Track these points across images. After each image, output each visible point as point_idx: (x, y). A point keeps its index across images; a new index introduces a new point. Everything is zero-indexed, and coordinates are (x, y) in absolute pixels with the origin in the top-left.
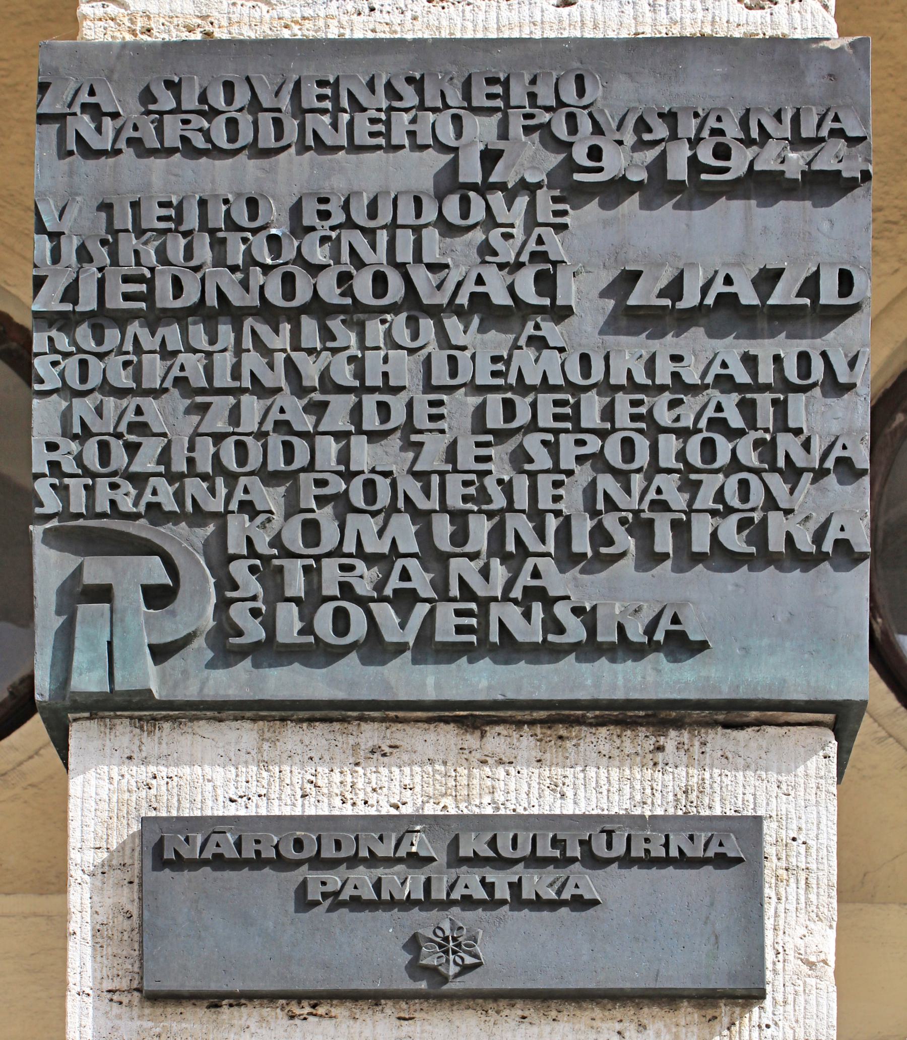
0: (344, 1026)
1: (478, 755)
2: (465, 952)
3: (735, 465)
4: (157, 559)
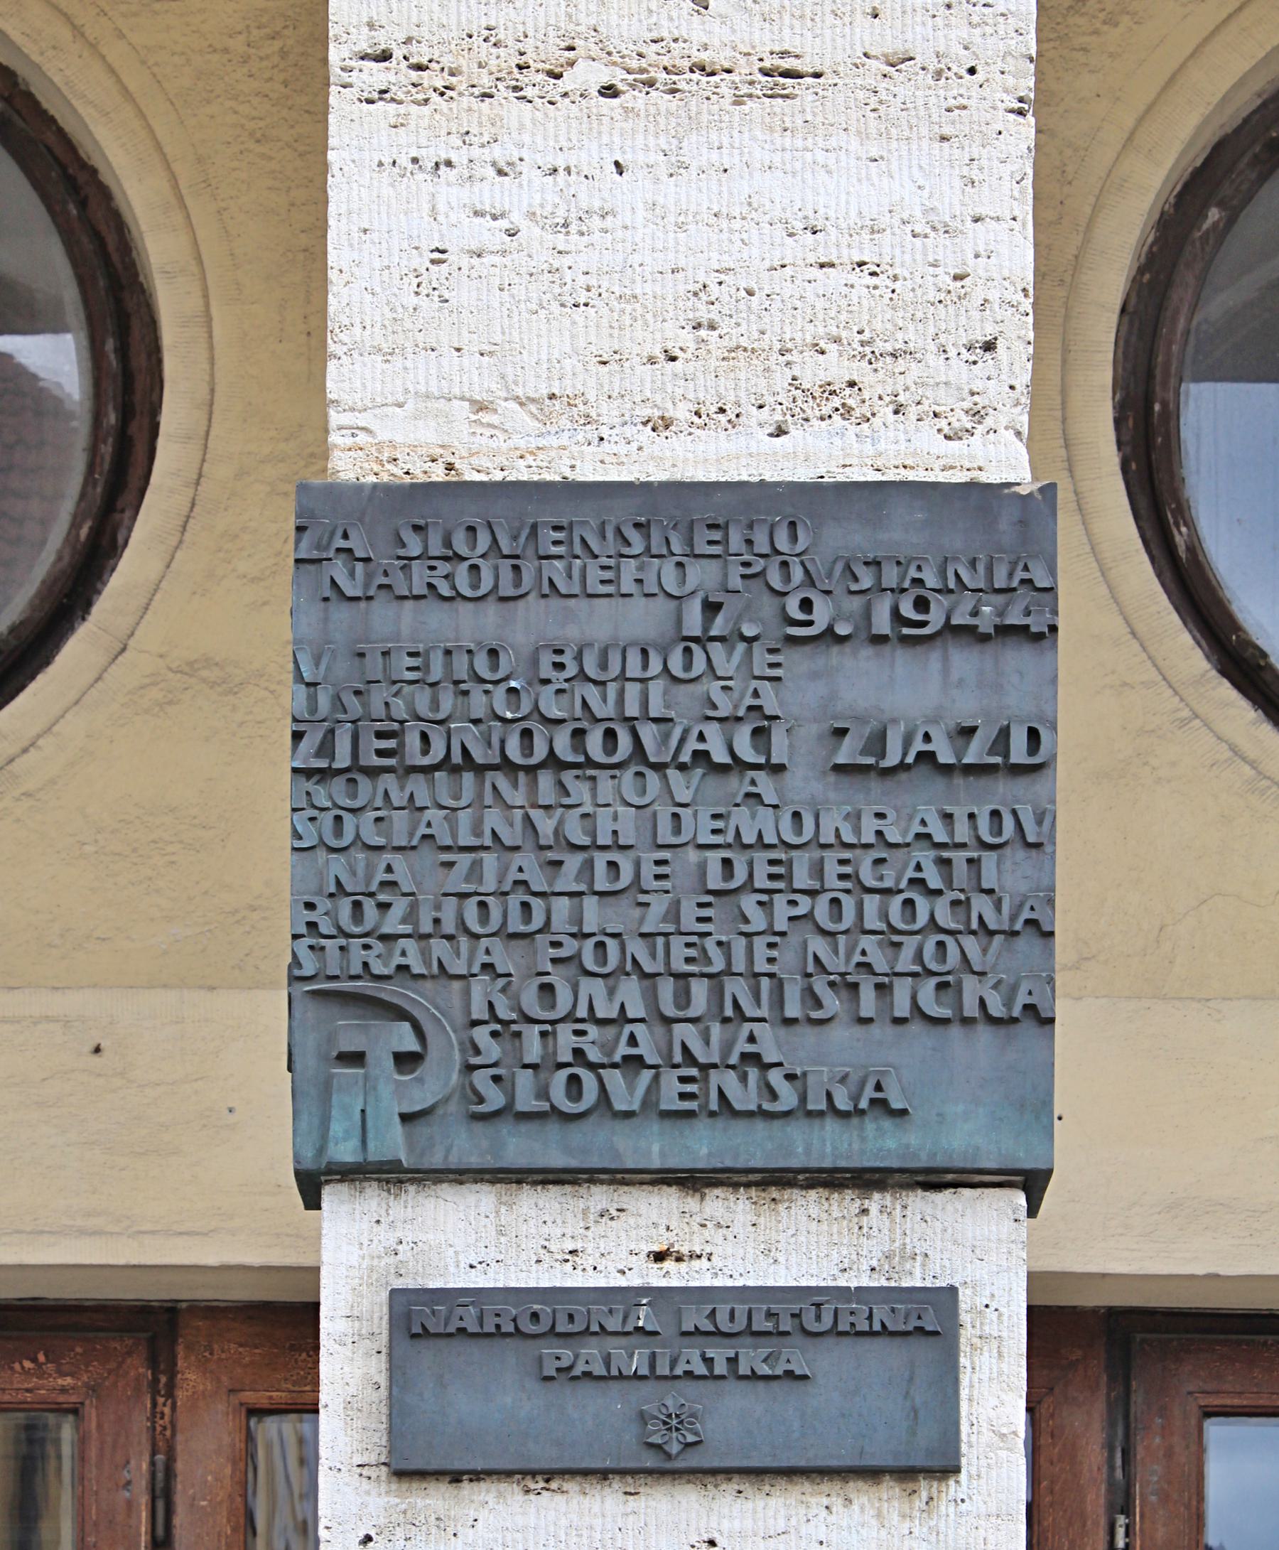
0: (575, 1501)
1: (698, 1219)
2: (687, 1429)
4: (406, 1026)
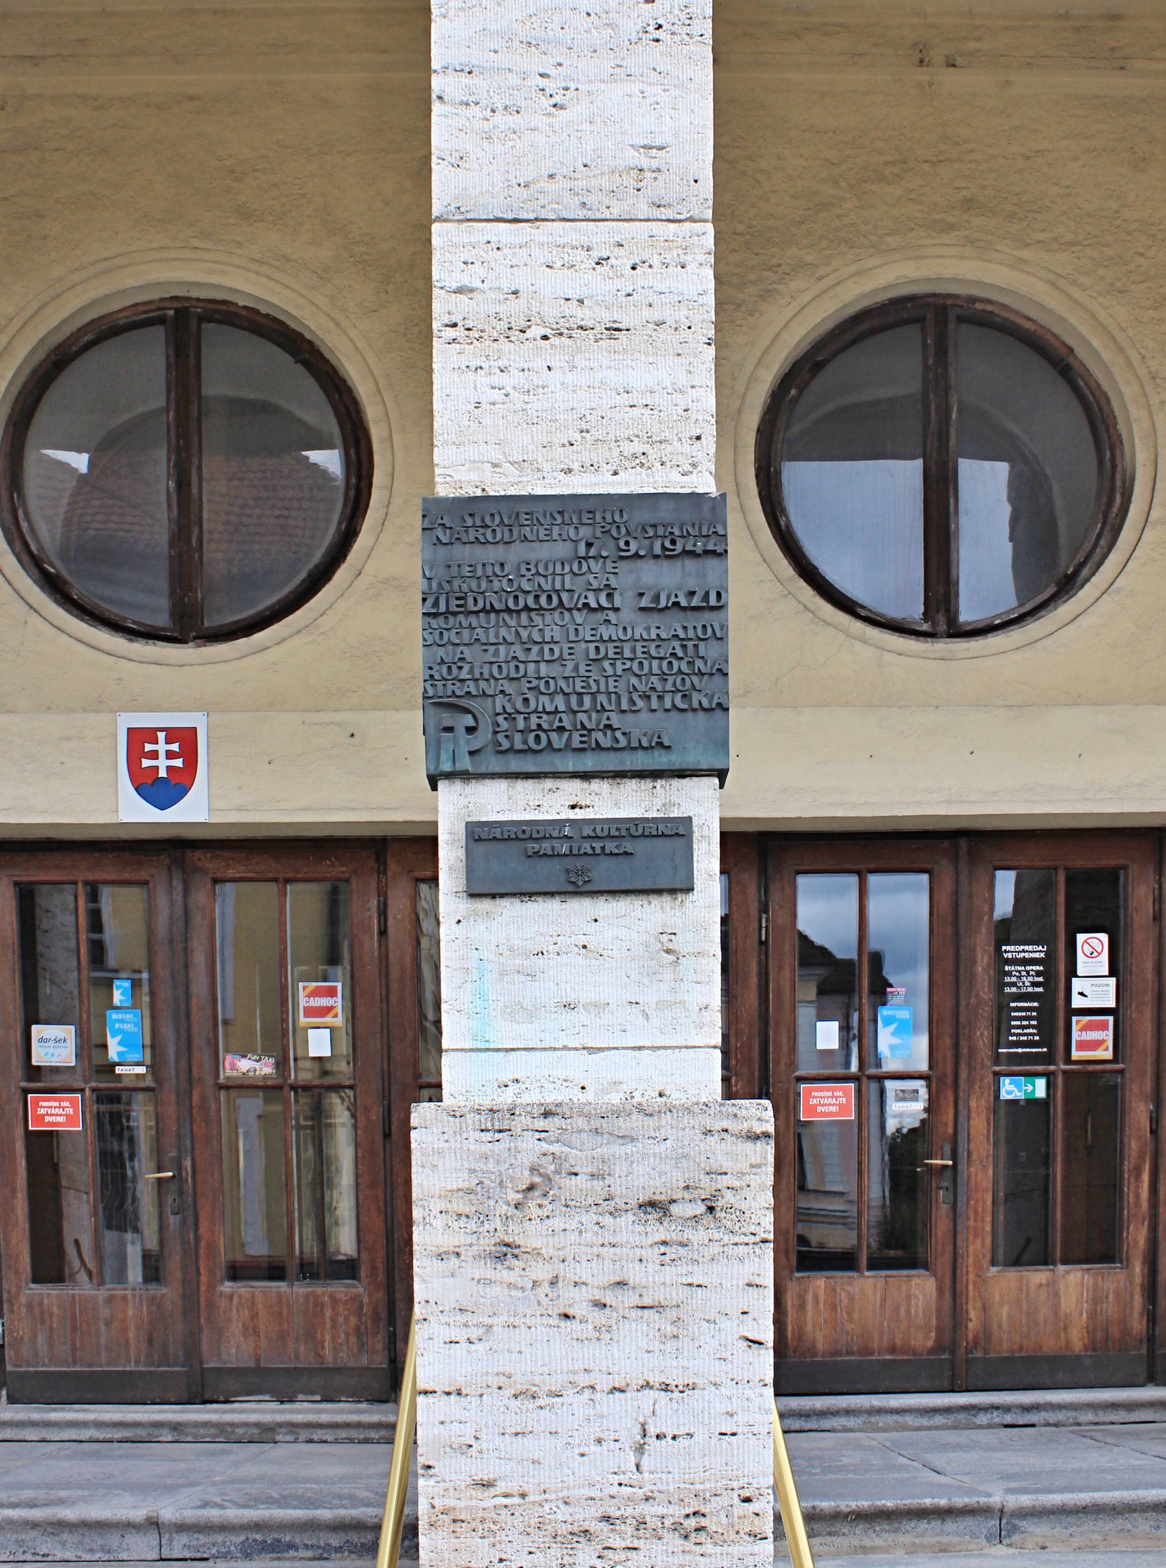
3: (680, 671)
